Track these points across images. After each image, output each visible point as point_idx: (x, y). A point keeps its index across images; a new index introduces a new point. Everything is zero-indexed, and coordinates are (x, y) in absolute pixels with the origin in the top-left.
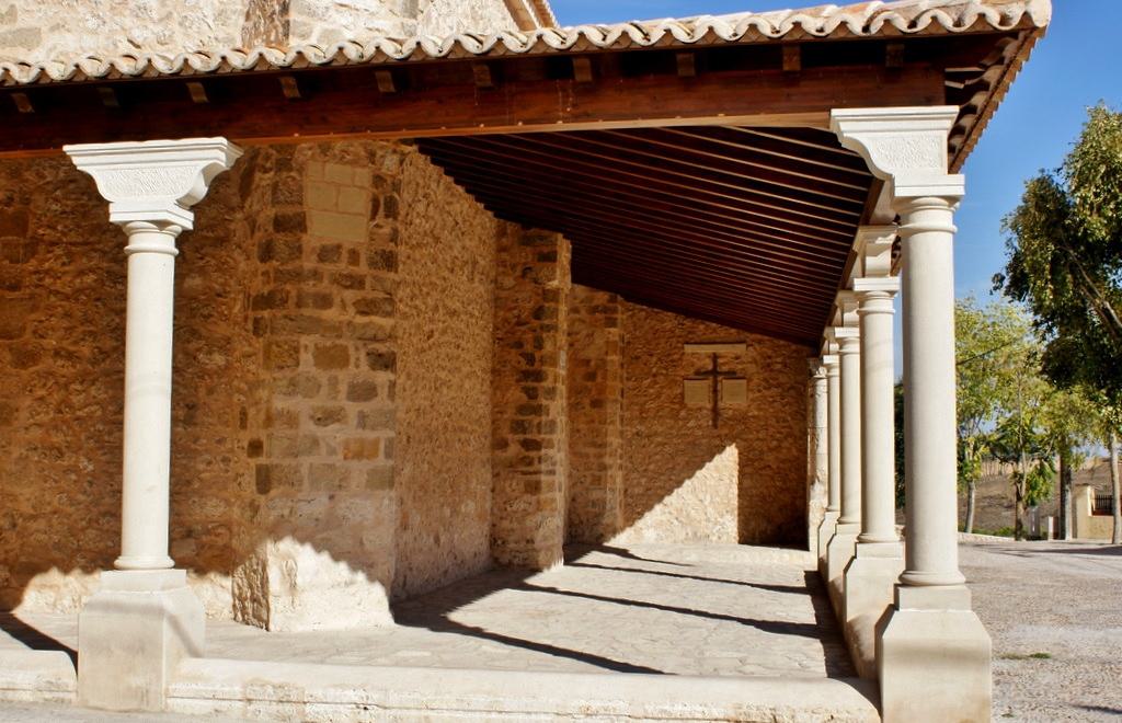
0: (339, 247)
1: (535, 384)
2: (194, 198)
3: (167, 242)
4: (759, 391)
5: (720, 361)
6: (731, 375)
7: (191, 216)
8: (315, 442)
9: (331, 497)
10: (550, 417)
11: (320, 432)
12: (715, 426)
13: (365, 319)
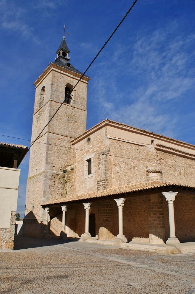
9: (156, 229)
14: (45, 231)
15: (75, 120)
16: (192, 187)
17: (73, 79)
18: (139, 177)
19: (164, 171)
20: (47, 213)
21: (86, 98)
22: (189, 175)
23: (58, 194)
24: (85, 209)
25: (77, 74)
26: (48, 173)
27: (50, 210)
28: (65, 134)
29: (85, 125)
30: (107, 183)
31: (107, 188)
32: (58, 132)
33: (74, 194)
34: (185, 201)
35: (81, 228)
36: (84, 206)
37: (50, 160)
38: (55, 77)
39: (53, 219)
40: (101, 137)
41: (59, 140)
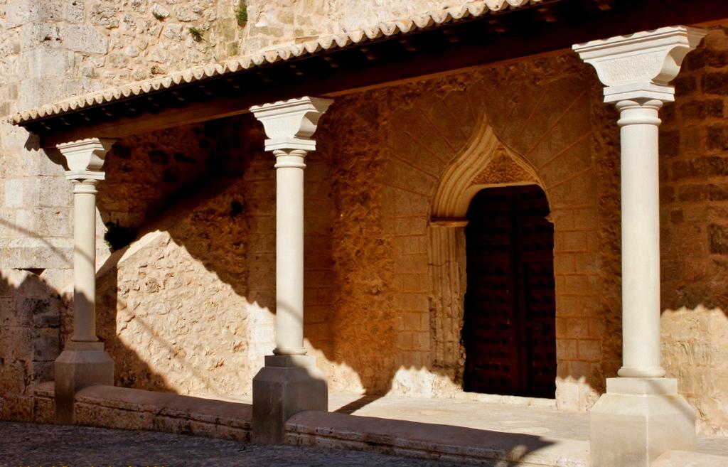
2: (668, 76)
3: (651, 116)
7: (672, 90)
14: (68, 358)
20: (79, 187)
23: (169, 25)
24: (271, 157)
27: (115, 160)
33: (304, 27)
35: (387, 316)
39: (135, 247)
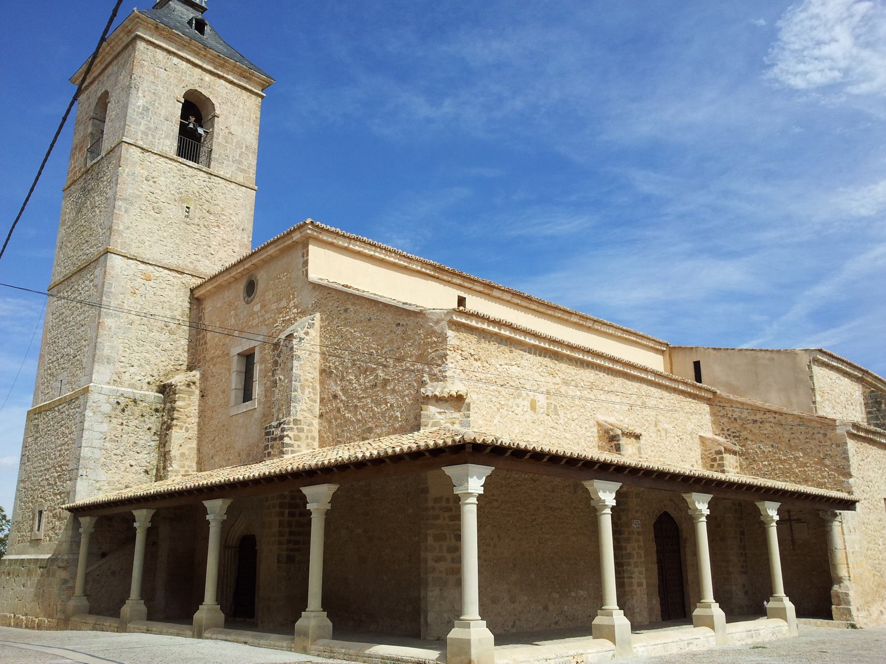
0: (442, 497)
1: (619, 536)
4: (815, 529)
5: (791, 513)
6: (799, 520)
8: (434, 569)
9: (441, 590)
10: (628, 551)
11: (436, 565)
12: (794, 549)
13: (453, 523)
15: (211, 217)
16: (542, 451)
17: (213, 78)
18: (398, 414)
19: (481, 396)
21: (255, 145)
22: (561, 413)
23: (133, 469)
25: (226, 61)
26: (100, 393)
27: (98, 525)
28: (173, 262)
29: (245, 236)
30: (296, 432)
31: (295, 448)
32: (147, 256)
34: (545, 496)
36: (205, 511)
37: (112, 348)
38: (146, 63)
40: (290, 278)
41: (151, 283)
